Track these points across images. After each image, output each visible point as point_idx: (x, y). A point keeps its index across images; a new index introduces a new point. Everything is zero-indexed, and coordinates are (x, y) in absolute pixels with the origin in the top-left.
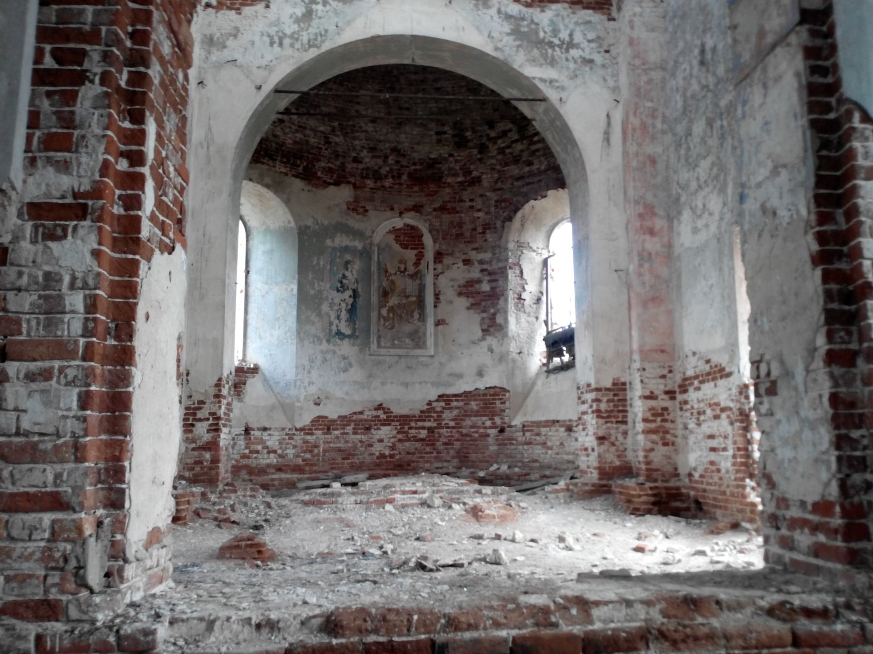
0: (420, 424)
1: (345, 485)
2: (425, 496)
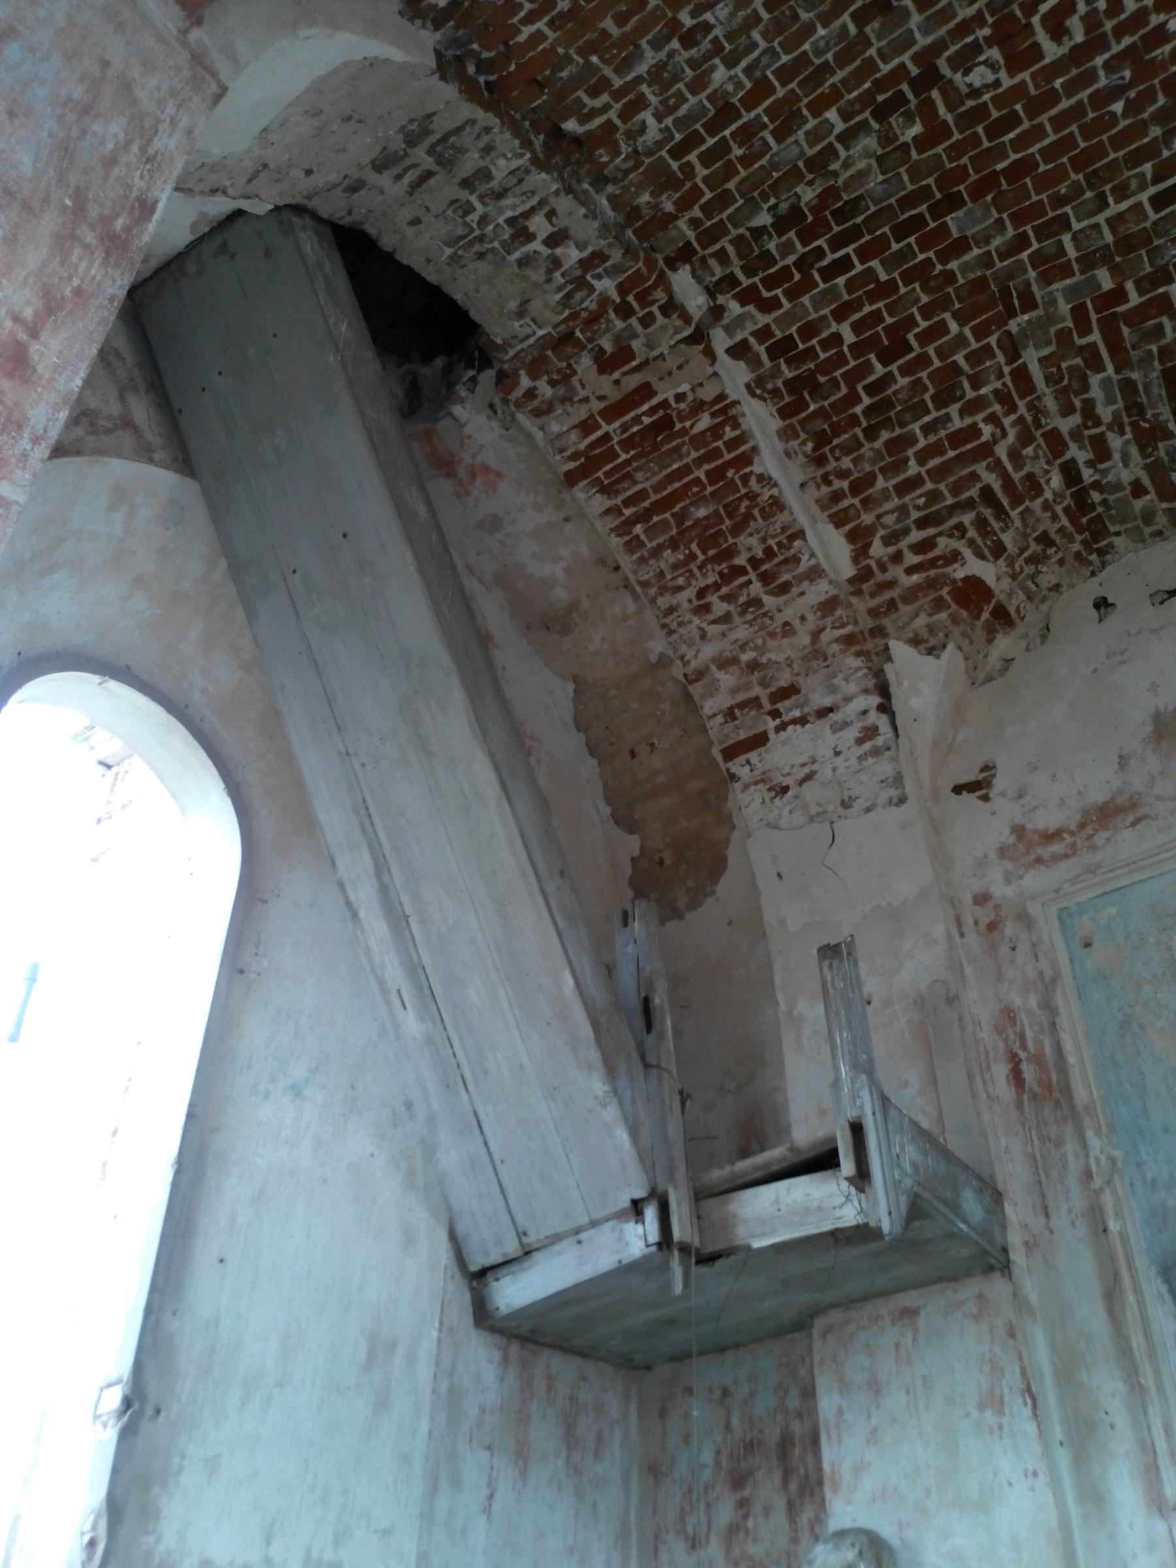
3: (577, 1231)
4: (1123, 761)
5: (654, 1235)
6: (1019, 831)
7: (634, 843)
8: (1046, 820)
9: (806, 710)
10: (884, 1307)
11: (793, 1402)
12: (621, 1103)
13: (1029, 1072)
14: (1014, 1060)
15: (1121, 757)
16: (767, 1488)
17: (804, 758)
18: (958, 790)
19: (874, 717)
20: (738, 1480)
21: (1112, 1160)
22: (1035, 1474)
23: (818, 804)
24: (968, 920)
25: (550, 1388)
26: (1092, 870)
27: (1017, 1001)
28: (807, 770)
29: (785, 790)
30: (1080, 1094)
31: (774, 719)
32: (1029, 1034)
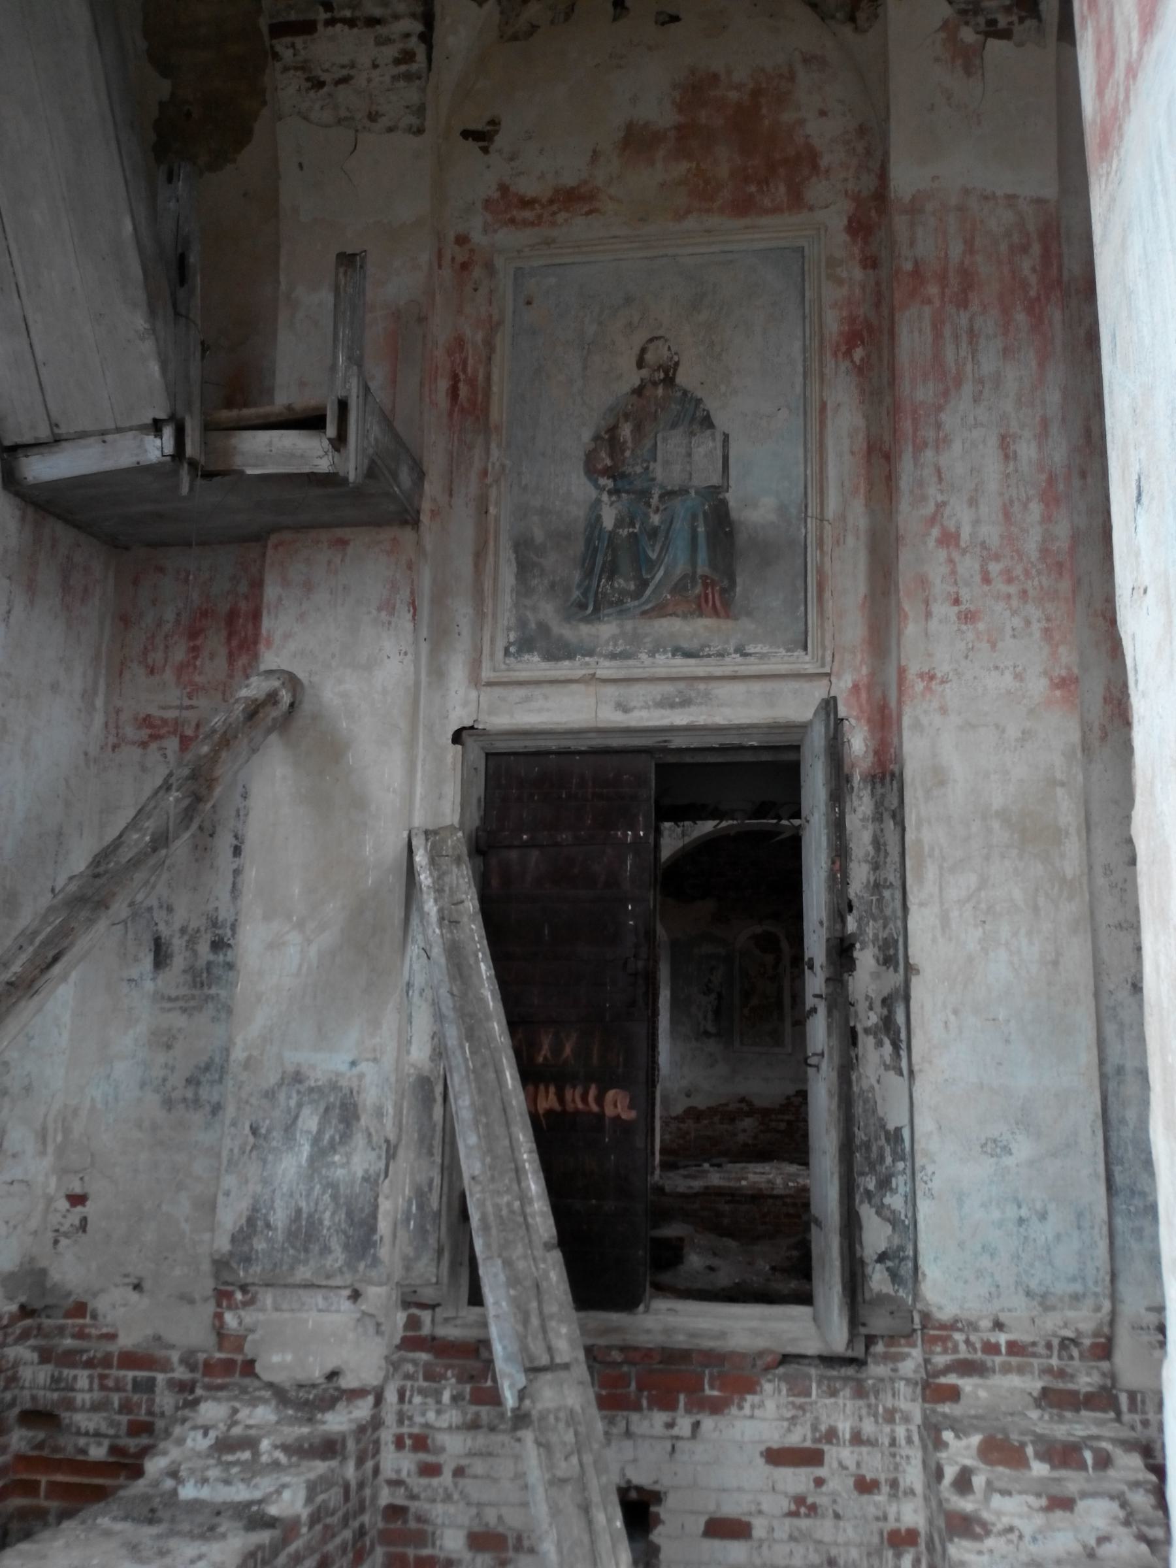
0: (780, 1117)
1: (712, 1165)
2: (771, 1176)
3: (104, 433)
4: (595, 155)
5: (169, 448)
7: (165, 87)
8: (527, 187)
9: (358, 13)
11: (243, 588)
12: (157, 340)
14: (455, 378)
15: (594, 152)
16: (215, 641)
17: (345, 60)
18: (466, 134)
19: (414, 43)
20: (194, 634)
21: (503, 467)
22: (406, 654)
23: (348, 109)
25: (53, 546)
26: (548, 242)
28: (345, 72)
29: (321, 84)
30: (494, 415)
31: (326, 11)
32: (470, 362)
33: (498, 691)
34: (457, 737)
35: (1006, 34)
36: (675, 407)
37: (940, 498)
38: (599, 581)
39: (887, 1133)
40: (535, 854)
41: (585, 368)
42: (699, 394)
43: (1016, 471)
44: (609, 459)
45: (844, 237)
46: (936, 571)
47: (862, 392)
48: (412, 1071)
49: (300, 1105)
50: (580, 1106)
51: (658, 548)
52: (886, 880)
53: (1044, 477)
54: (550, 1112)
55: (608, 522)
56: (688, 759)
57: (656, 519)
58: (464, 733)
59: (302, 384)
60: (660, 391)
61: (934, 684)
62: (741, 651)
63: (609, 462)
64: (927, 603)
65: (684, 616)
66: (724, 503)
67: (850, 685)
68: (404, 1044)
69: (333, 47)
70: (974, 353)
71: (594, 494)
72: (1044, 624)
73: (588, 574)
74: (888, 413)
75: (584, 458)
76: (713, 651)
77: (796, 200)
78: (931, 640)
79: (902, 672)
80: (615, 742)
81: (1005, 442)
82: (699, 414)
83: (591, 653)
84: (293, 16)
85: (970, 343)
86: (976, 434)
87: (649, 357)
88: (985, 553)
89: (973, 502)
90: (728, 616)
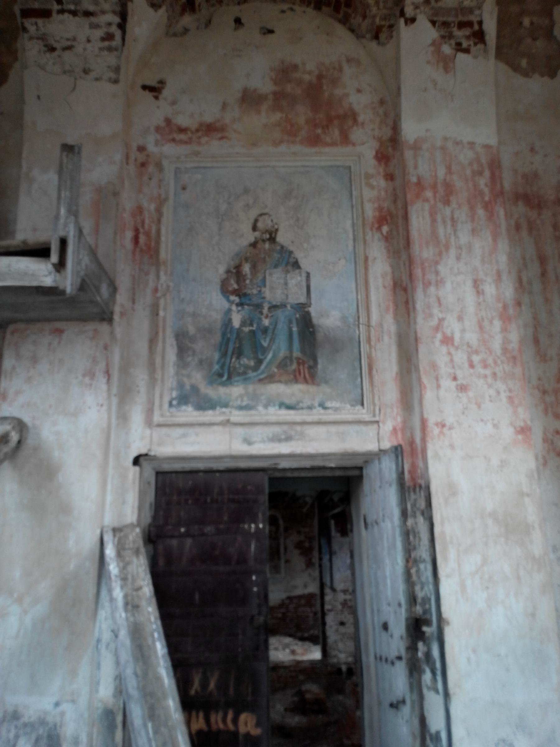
4: (224, 106)
6: (168, 121)
8: (182, 121)
10: (48, 326)
13: (142, 239)
17: (69, 36)
18: (145, 87)
19: (114, 29)
21: (168, 287)
24: (132, 157)
26: (197, 154)
27: (145, 204)
28: (69, 43)
29: (52, 49)
30: (163, 255)
32: (147, 221)
33: (164, 430)
34: (136, 461)
35: (467, 51)
36: (276, 255)
37: (440, 316)
38: (231, 359)
39: (431, 735)
40: (189, 542)
41: (220, 229)
42: (291, 248)
43: (484, 301)
44: (236, 284)
45: (373, 162)
46: (442, 360)
47: (388, 251)
48: (100, 705)
49: (17, 737)
50: (221, 726)
51: (268, 339)
52: (420, 557)
53: (500, 305)
54: (200, 733)
55: (236, 322)
56: (289, 475)
57: (266, 322)
58: (141, 460)
59: (35, 230)
60: (267, 245)
61: (445, 430)
62: (322, 405)
63: (236, 286)
64: (437, 379)
65: (286, 383)
66: (308, 313)
67: (391, 428)
68: (95, 684)
69: (62, 27)
70: (455, 231)
71: (226, 305)
72: (508, 394)
73: (224, 355)
74: (404, 264)
75: (220, 283)
76: (305, 405)
77: (345, 139)
78: (441, 402)
79: (424, 423)
80: (243, 464)
81: (476, 284)
82: (292, 260)
83: (226, 406)
84: (36, 6)
85: (453, 226)
86: (460, 278)
87: (260, 225)
88: (469, 349)
89: (460, 319)
90: (313, 383)
